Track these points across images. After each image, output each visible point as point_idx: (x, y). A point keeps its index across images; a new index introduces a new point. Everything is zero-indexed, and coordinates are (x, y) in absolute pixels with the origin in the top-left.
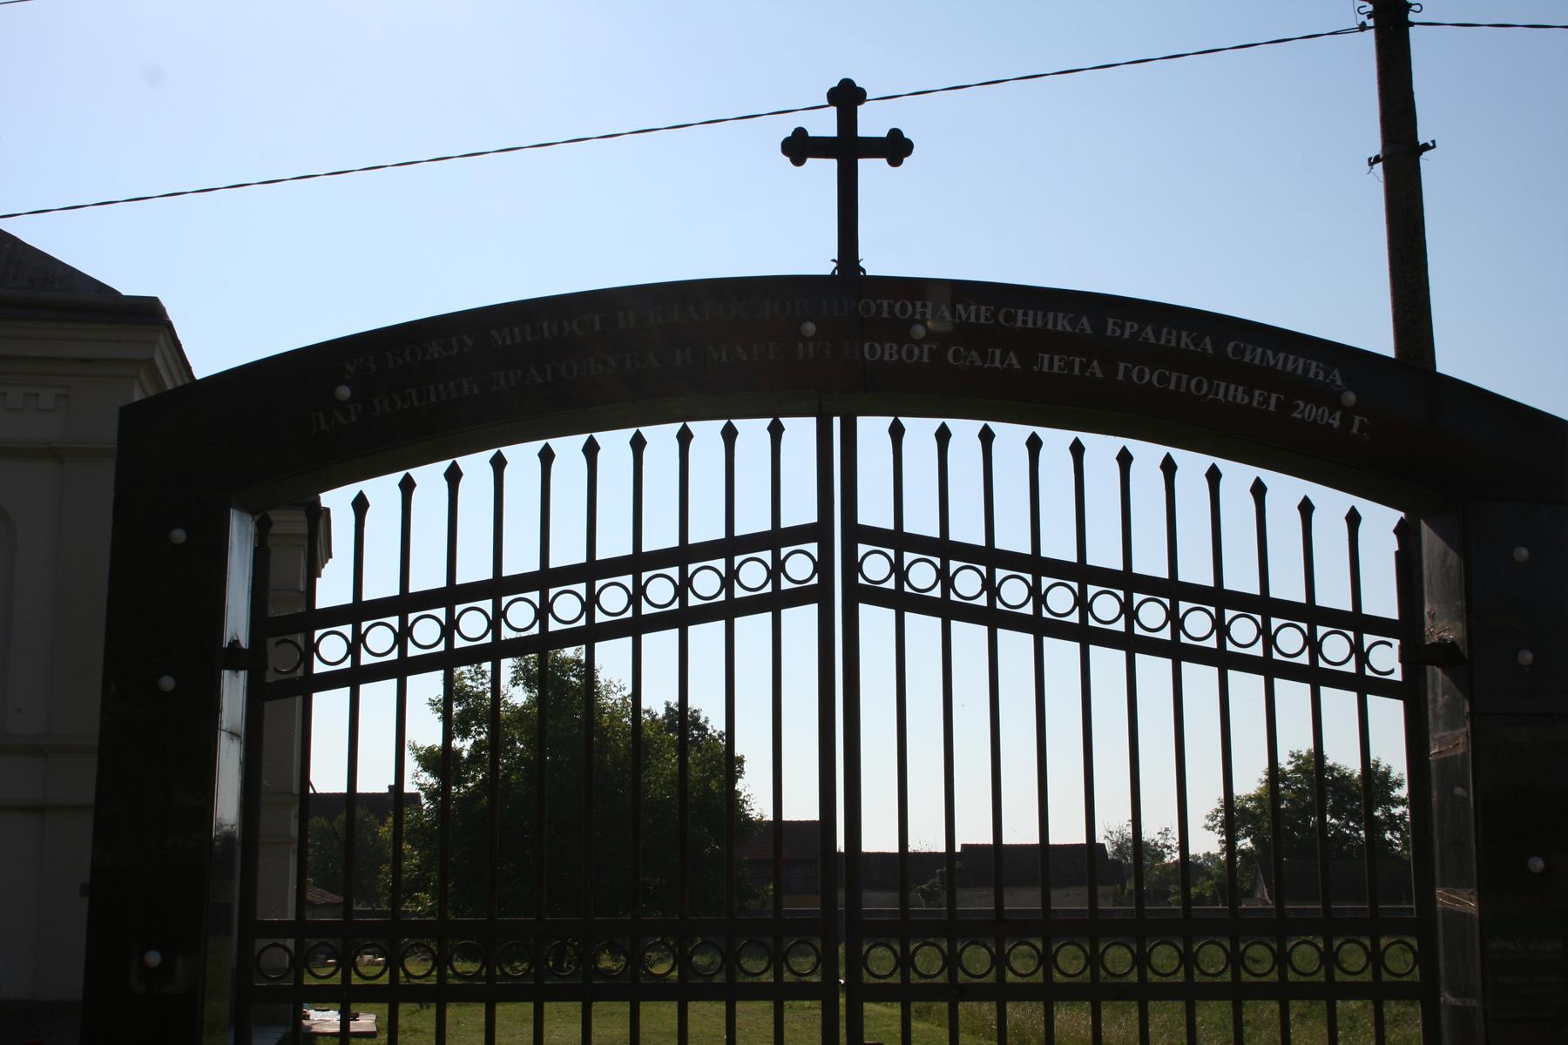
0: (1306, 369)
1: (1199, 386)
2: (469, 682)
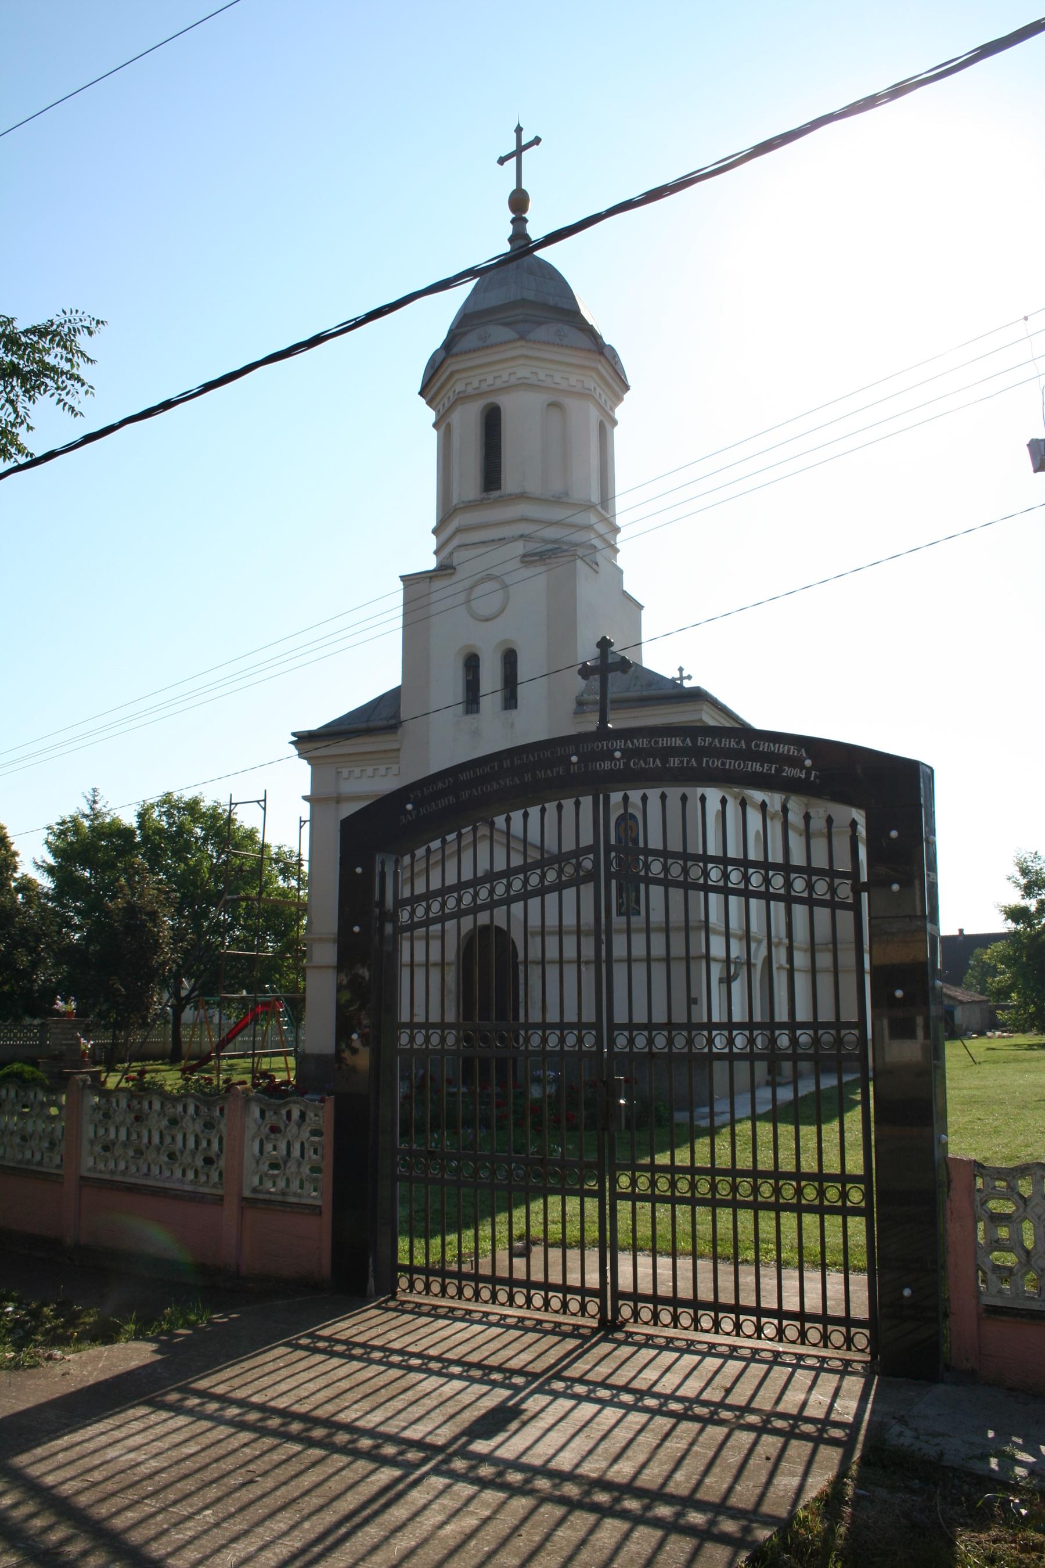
0: (789, 751)
1: (739, 765)
2: (1029, 864)
